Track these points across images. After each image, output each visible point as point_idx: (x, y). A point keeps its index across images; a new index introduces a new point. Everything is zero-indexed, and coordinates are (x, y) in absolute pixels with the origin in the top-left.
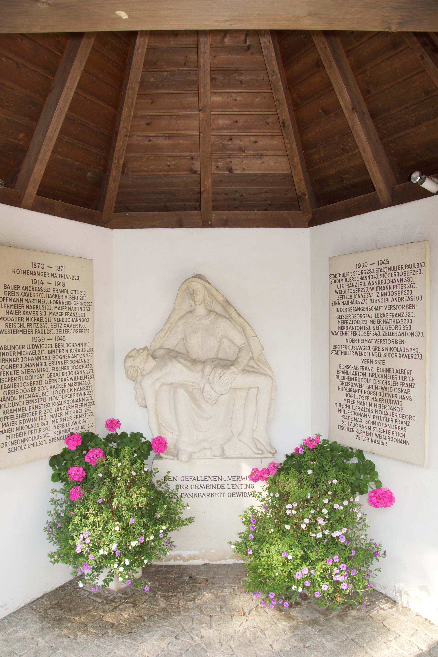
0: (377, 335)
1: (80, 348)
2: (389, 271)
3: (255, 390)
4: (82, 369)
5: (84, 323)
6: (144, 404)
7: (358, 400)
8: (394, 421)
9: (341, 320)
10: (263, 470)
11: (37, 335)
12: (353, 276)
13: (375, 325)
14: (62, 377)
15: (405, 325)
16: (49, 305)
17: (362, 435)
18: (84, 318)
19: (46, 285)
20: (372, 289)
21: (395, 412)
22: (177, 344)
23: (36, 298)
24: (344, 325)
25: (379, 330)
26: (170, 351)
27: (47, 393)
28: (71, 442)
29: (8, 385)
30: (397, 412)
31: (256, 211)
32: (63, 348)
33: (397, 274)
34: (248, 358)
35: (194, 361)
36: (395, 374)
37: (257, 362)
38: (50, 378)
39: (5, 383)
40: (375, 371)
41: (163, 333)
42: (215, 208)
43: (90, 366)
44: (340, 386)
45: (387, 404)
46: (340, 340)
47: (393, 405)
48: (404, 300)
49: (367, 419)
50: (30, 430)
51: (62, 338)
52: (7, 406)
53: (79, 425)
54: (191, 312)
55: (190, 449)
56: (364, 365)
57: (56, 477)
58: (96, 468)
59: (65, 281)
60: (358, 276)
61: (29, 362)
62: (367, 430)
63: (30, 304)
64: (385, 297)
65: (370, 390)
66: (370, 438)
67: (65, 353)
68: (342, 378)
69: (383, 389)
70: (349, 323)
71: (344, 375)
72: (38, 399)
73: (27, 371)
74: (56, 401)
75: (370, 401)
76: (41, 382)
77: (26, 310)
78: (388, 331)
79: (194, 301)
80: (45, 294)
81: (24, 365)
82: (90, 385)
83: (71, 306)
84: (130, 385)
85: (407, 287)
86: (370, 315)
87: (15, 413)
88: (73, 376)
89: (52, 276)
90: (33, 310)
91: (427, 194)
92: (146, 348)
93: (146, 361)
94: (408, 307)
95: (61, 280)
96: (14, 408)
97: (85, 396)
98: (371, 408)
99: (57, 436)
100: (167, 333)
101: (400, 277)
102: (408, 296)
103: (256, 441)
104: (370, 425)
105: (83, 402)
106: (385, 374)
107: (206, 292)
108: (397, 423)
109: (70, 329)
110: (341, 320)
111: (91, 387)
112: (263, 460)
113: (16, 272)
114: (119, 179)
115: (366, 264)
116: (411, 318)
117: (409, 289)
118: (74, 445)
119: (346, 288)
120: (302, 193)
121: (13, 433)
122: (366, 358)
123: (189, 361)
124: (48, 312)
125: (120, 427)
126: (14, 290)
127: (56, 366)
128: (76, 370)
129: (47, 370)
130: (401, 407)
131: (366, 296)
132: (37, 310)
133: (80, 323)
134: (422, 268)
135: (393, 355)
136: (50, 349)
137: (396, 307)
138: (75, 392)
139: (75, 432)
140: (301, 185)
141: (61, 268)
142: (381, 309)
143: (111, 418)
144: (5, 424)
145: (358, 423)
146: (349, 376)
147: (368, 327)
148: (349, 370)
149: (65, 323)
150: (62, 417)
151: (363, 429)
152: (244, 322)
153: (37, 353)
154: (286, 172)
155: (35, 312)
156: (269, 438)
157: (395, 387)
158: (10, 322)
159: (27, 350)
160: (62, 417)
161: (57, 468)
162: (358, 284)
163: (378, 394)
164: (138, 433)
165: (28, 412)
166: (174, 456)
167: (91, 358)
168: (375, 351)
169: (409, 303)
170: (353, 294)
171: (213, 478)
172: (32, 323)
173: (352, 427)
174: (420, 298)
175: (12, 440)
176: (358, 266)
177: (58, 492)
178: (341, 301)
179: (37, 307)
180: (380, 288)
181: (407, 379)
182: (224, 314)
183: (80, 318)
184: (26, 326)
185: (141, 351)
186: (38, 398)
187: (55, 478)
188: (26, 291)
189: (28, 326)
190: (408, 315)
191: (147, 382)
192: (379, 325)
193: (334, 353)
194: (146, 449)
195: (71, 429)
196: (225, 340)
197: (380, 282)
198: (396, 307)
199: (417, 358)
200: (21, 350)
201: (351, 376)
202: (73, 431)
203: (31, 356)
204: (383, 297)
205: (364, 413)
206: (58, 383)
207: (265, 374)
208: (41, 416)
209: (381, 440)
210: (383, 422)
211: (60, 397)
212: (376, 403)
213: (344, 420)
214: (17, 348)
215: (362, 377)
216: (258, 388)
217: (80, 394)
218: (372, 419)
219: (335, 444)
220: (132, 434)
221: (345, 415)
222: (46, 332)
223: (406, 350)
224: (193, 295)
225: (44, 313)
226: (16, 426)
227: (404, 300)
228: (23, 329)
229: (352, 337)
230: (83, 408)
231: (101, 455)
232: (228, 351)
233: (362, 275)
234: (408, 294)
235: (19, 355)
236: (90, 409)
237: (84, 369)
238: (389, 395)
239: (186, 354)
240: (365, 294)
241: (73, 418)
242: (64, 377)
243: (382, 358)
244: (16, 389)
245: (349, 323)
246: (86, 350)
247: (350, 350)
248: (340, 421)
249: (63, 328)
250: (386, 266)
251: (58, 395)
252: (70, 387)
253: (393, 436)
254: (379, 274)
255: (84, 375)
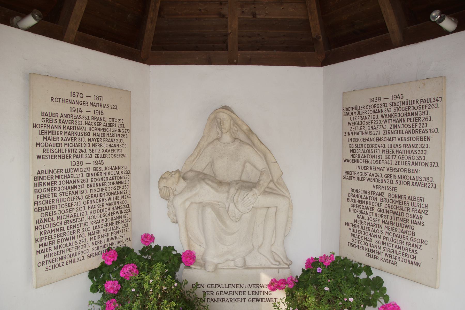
0: (389, 163)
1: (118, 171)
2: (403, 105)
3: (274, 210)
4: (119, 190)
5: (122, 148)
6: (175, 220)
7: (369, 221)
8: (405, 243)
9: (353, 149)
10: (280, 280)
11: (76, 160)
12: (366, 109)
13: (388, 154)
14: (100, 198)
15: (419, 155)
16: (88, 131)
17: (372, 254)
18: (122, 143)
19: (84, 114)
20: (385, 122)
21: (406, 235)
22: (206, 167)
23: (75, 125)
24: (356, 153)
25: (392, 160)
26: (199, 173)
27: (85, 213)
28: (107, 257)
29: (46, 207)
30: (408, 235)
31: (275, 52)
32: (101, 171)
33: (412, 108)
34: (269, 181)
35: (220, 183)
36: (407, 200)
37: (276, 184)
38: (88, 199)
39: (42, 205)
40: (386, 196)
41: (193, 158)
42: (240, 49)
43: (127, 187)
44: (351, 207)
45: (398, 228)
46: (352, 167)
47: (404, 229)
48: (419, 132)
49: (377, 239)
50: (69, 248)
51: (100, 162)
52: (45, 227)
53: (117, 240)
54: (218, 139)
55: (216, 261)
56: (375, 190)
57: (94, 289)
58: (130, 282)
59: (104, 110)
60: (371, 109)
61: (68, 185)
62: (377, 250)
63: (68, 131)
64: (399, 129)
65: (381, 213)
66: (380, 256)
67: (103, 176)
68: (353, 201)
69: (394, 213)
70: (361, 152)
71: (355, 198)
72: (77, 219)
73: (65, 193)
74: (94, 220)
75: (380, 223)
76: (79, 203)
77: (64, 136)
78: (401, 160)
79: (221, 129)
80: (84, 121)
81: (62, 188)
82: (127, 204)
83: (110, 133)
84: (164, 203)
85: (421, 120)
86: (383, 146)
87: (53, 234)
88: (111, 196)
89: (91, 105)
90: (71, 137)
91: (445, 33)
92: (178, 171)
93: (178, 183)
94: (422, 139)
95: (99, 109)
96: (51, 228)
97: (122, 214)
98: (381, 230)
99: (95, 252)
100: (196, 157)
101: (414, 111)
102: (422, 129)
103: (274, 254)
104: (379, 245)
105: (121, 220)
106: (397, 200)
107: (232, 122)
108: (407, 245)
109: (108, 153)
110: (353, 149)
111: (127, 206)
112: (280, 270)
113: (54, 100)
114: (156, 20)
115: (380, 99)
116: (426, 149)
117: (424, 122)
118: (110, 261)
119: (359, 121)
120: (317, 36)
121: (51, 252)
122: (378, 184)
123: (216, 183)
124: (86, 138)
125: (154, 242)
126: (52, 118)
127: (94, 188)
128: (114, 191)
129: (85, 191)
130: (413, 231)
131: (379, 127)
132: (76, 136)
133: (118, 148)
134: (439, 103)
135: (405, 183)
136: (89, 172)
137: (409, 138)
138: (113, 211)
139: (112, 247)
140: (316, 28)
141: (100, 98)
142: (394, 140)
143: (146, 233)
144: (42, 244)
145: (368, 242)
146: (360, 199)
147: (381, 157)
148: (361, 194)
149: (103, 148)
150: (100, 234)
151: (372, 248)
152: (266, 149)
153: (76, 176)
154: (303, 18)
155: (73, 139)
156: (285, 251)
157: (407, 212)
158: (48, 148)
159: (65, 174)
160: (100, 234)
161: (96, 280)
162: (371, 117)
163: (389, 217)
164: (170, 246)
165: (66, 231)
166: (201, 266)
167: (128, 179)
168: (387, 179)
169: (423, 135)
170: (365, 126)
171: (236, 286)
172: (71, 148)
173: (362, 245)
174: (436, 131)
175: (50, 258)
176: (371, 100)
177: (96, 303)
178: (354, 131)
179: (75, 133)
180: (393, 121)
181: (420, 206)
182: (247, 141)
183: (118, 143)
184: (64, 151)
185: (173, 173)
186: (77, 218)
187: (94, 289)
188: (65, 119)
189: (66, 151)
190: (422, 146)
191: (178, 201)
192: (392, 154)
193: (346, 178)
194: (177, 262)
195: (109, 245)
196: (248, 164)
197: (394, 115)
198: (410, 139)
199: (431, 186)
200: (59, 174)
201: (362, 200)
202: (111, 246)
203: (69, 179)
204: (397, 129)
205: (374, 233)
206: (96, 204)
207: (283, 196)
208: (79, 234)
209: (391, 259)
210: (393, 243)
211: (98, 216)
212: (386, 225)
213: (355, 238)
214: (55, 172)
215: (373, 201)
216: (277, 207)
217: (117, 213)
218: (382, 239)
219: (346, 260)
220: (165, 247)
221: (356, 234)
222: (85, 156)
223: (419, 179)
224: (220, 124)
225: (83, 139)
226: (54, 245)
227: (419, 132)
228: (61, 154)
229: (364, 164)
230: (120, 225)
231: (135, 270)
232: (251, 174)
233: (375, 109)
234: (423, 127)
235: (57, 179)
236: (126, 225)
237: (121, 190)
238: (400, 219)
239: (213, 176)
240: (378, 126)
241: (110, 234)
242: (102, 198)
243: (394, 185)
244: (54, 211)
245: (361, 152)
246: (124, 173)
247: (362, 176)
248: (350, 239)
249: (101, 153)
250: (400, 100)
251: (96, 214)
252: (107, 207)
253: (403, 257)
254: (392, 108)
255: (121, 195)
